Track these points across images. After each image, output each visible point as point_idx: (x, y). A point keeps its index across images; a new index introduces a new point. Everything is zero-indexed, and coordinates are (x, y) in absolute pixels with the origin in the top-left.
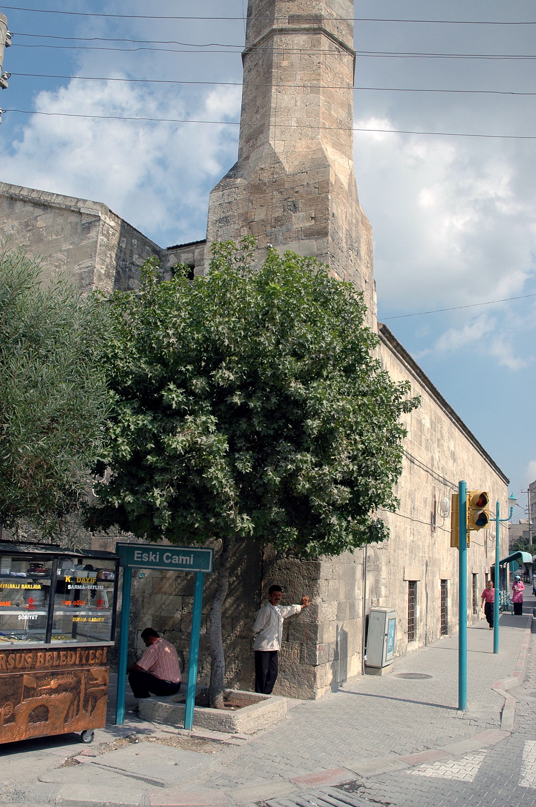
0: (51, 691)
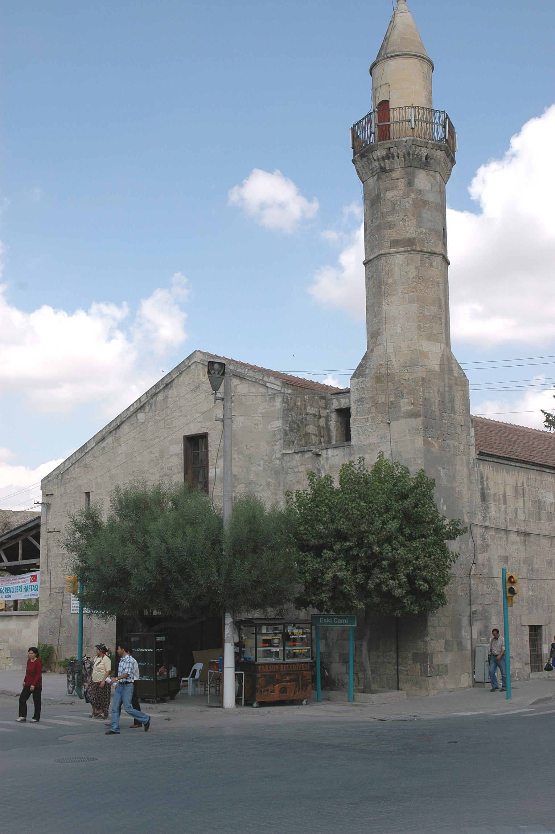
0: (287, 681)
